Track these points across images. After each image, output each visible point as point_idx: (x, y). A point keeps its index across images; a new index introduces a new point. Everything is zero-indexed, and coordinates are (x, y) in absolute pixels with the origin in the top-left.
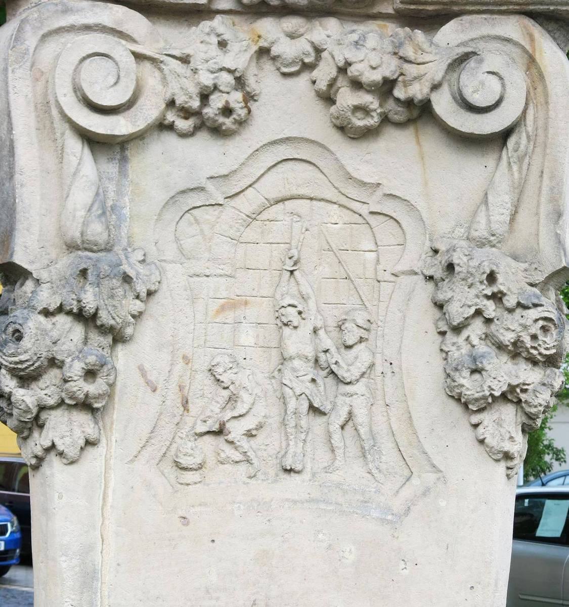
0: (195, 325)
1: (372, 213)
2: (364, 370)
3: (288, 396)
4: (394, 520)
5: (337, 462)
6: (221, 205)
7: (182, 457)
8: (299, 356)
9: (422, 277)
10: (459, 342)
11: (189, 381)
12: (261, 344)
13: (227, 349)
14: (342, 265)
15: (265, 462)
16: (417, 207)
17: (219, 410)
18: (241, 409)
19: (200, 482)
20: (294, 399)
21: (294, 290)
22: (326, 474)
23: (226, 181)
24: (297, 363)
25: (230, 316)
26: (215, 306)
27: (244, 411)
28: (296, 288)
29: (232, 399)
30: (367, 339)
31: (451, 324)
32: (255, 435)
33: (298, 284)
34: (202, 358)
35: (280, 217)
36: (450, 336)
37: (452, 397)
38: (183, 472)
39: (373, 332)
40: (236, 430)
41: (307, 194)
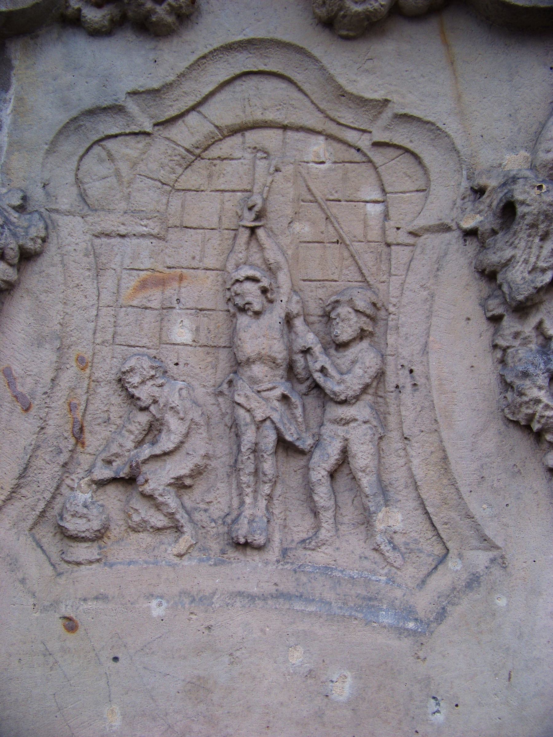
0: (98, 310)
1: (377, 144)
2: (369, 381)
3: (243, 423)
4: (421, 629)
5: (323, 531)
6: (148, 134)
7: (69, 518)
8: (261, 358)
9: (457, 234)
10: (526, 331)
11: (85, 397)
12: (203, 341)
13: (148, 349)
14: (332, 223)
15: (205, 531)
16: (447, 130)
17: (133, 445)
18: (166, 443)
19: (98, 561)
20: (253, 427)
21: (256, 258)
22: (304, 552)
23: (158, 99)
24: (258, 370)
25: (155, 297)
26: (131, 282)
27: (171, 446)
28: (258, 256)
29: (154, 429)
30: (372, 334)
31: (513, 299)
32: (190, 487)
33: (262, 248)
34: (108, 361)
35: (237, 154)
36: (510, 324)
37: (516, 423)
38: (72, 544)
39: (381, 323)
40: (158, 478)
41: (278, 121)
